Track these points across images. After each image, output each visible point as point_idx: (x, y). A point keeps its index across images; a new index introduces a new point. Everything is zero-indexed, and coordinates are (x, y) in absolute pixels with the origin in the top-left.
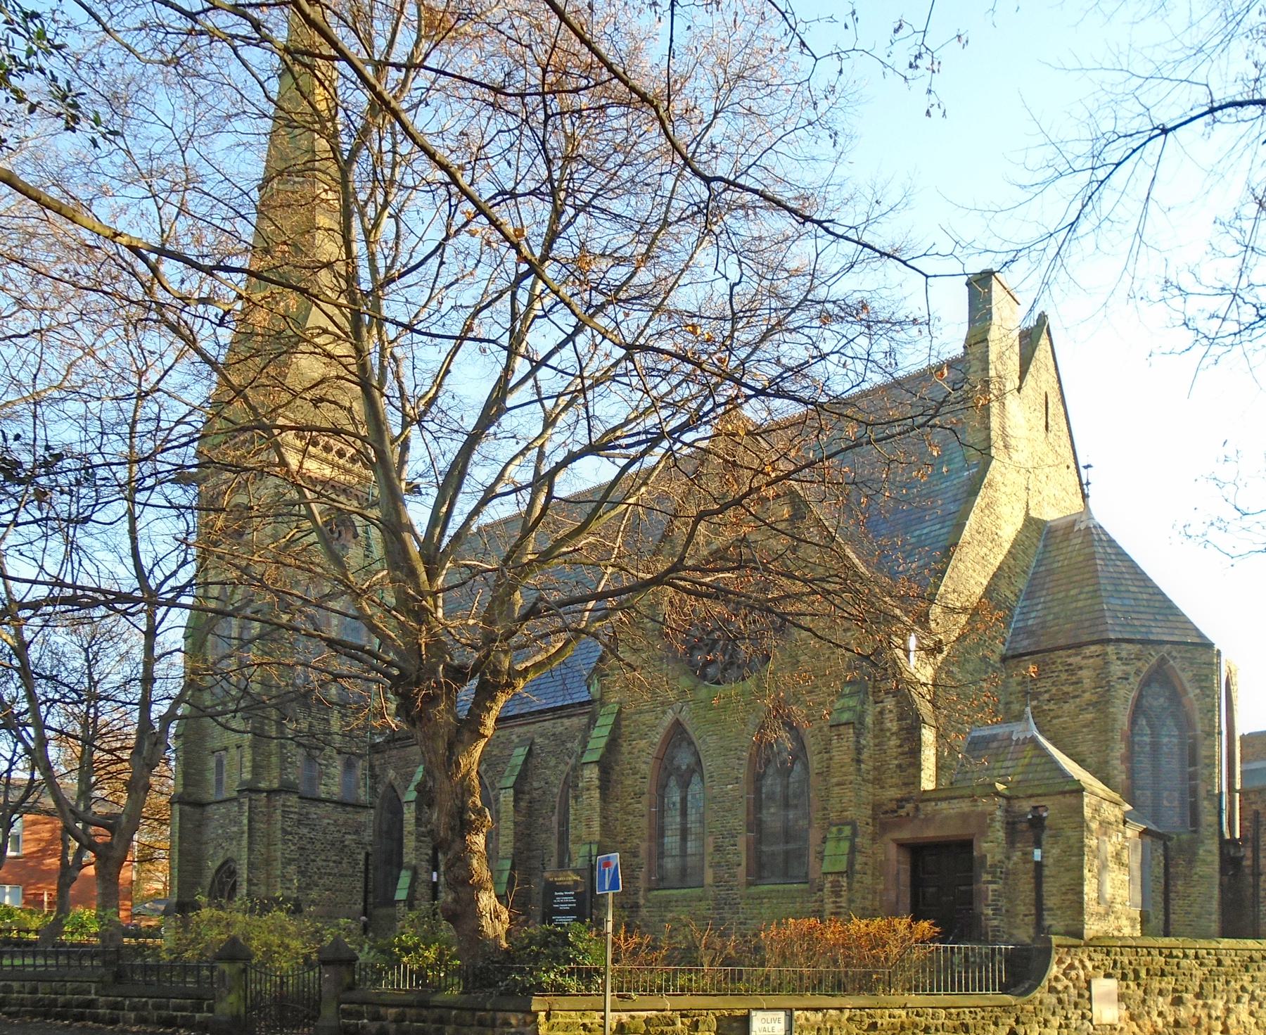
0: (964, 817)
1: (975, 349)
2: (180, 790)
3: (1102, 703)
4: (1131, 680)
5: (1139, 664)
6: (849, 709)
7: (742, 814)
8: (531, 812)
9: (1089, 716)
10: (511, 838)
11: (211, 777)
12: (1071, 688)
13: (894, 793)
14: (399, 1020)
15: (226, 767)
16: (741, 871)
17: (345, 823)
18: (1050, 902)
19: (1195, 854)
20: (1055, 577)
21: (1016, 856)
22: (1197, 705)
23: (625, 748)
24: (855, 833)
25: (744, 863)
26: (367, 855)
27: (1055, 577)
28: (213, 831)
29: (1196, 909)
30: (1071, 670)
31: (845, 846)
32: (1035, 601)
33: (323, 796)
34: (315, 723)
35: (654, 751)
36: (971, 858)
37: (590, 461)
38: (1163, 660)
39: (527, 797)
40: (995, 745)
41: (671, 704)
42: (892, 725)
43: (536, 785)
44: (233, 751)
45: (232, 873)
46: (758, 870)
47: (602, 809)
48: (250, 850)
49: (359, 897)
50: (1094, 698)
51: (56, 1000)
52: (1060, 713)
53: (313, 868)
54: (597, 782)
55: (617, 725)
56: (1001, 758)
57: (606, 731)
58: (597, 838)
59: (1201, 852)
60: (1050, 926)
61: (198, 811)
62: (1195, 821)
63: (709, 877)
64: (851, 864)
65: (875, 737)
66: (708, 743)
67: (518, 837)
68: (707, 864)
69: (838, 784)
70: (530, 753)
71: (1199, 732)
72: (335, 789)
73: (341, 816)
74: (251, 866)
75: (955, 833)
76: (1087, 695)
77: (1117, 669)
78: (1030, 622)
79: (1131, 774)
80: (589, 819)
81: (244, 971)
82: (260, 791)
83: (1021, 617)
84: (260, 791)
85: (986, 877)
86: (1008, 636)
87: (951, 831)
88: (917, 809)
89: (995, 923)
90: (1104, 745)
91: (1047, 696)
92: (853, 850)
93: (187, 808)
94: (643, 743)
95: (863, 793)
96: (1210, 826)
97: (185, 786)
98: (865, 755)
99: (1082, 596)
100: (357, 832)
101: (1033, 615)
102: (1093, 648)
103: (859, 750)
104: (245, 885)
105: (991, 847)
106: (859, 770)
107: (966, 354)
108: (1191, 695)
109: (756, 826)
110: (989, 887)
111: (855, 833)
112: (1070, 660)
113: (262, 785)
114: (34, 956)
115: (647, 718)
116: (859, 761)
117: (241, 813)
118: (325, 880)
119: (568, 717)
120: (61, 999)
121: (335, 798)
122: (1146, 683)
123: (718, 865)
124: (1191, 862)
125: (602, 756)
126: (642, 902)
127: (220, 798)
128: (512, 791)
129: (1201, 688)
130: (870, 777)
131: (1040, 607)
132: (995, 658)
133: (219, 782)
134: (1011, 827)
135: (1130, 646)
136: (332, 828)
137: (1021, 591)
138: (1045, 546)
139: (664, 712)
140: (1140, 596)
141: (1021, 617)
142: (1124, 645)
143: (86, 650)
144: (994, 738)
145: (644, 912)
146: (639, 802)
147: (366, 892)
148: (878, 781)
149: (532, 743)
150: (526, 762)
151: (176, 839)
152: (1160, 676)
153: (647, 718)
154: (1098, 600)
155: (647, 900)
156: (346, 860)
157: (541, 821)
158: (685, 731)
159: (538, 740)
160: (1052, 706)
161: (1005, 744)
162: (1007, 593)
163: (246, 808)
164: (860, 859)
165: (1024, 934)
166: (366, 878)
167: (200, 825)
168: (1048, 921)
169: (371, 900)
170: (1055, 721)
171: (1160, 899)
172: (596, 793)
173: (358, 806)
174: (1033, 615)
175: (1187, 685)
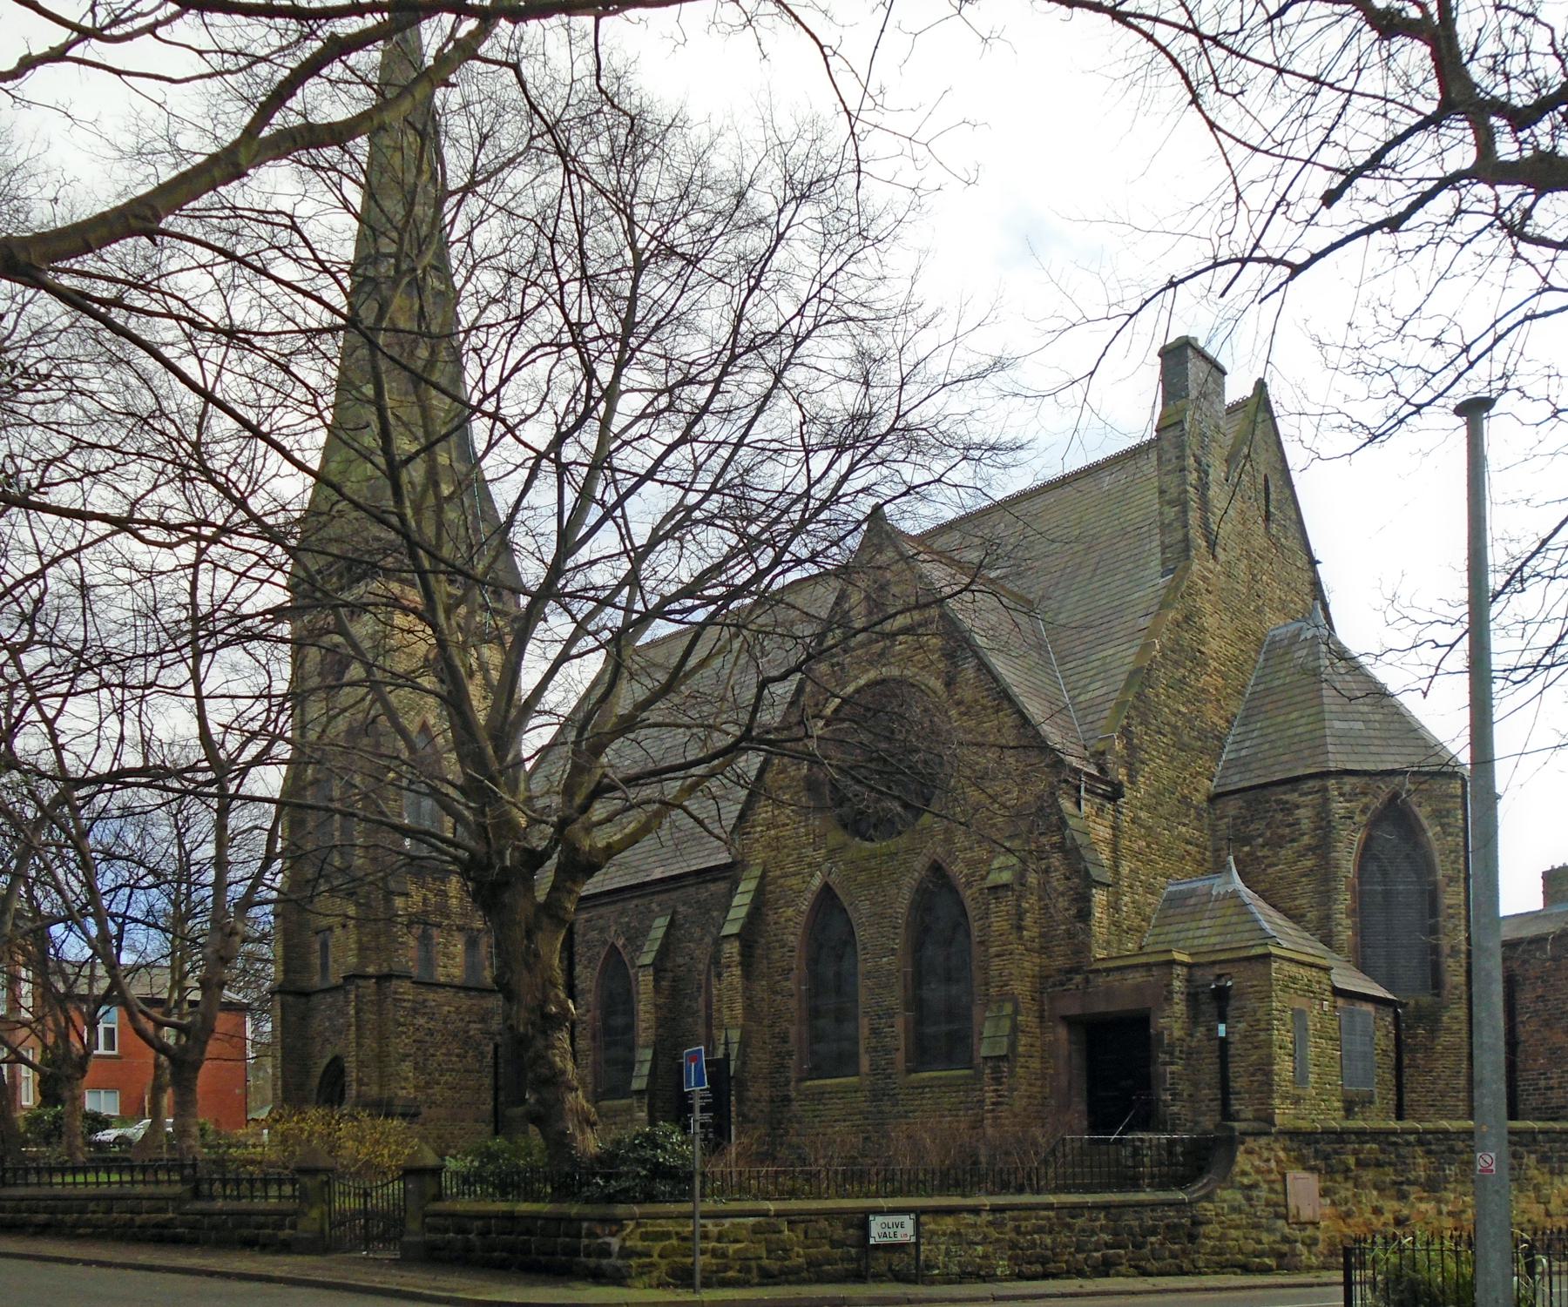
0: (1138, 989)
1: (1170, 434)
2: (281, 977)
3: (1323, 845)
4: (1357, 819)
5: (1365, 800)
6: (1007, 868)
7: (898, 991)
8: (675, 992)
9: (1309, 863)
10: (652, 1023)
11: (316, 960)
12: (1287, 830)
13: (1060, 962)
14: (484, 1233)
15: (332, 950)
16: (900, 1057)
17: (469, 1011)
18: (1238, 1084)
19: (1438, 1020)
20: (1275, 698)
21: (1201, 1032)
22: (1436, 845)
23: (772, 917)
24: (1016, 1012)
25: (902, 1046)
26: (496, 1047)
27: (1275, 698)
28: (319, 1023)
29: (1441, 1085)
30: (1288, 809)
31: (1006, 1025)
32: (1252, 727)
33: (442, 979)
34: (430, 896)
35: (802, 919)
36: (1148, 1037)
37: (570, 669)
38: (1395, 796)
39: (671, 974)
40: (1192, 901)
41: (818, 866)
42: (1057, 881)
43: (680, 960)
44: (338, 931)
45: (342, 1072)
46: (922, 1053)
47: (746, 989)
48: (359, 1045)
49: (488, 1096)
50: (1313, 842)
51: (132, 1220)
52: (1274, 860)
53: (432, 1065)
54: (737, 958)
55: (760, 892)
56: (1198, 916)
57: (747, 899)
58: (741, 1022)
59: (1445, 1019)
60: (1238, 1112)
61: (303, 1000)
62: (1436, 982)
63: (865, 1063)
64: (1013, 1045)
65: (1041, 899)
66: (860, 909)
67: (661, 1023)
68: (862, 1050)
69: (998, 956)
70: (672, 925)
71: (1440, 877)
72: (456, 972)
73: (464, 1001)
74: (361, 1064)
75: (1133, 1007)
76: (1306, 840)
77: (1339, 807)
78: (1243, 753)
79: (1361, 931)
80: (732, 1001)
81: (327, 1183)
82: (367, 977)
83: (1235, 747)
84: (367, 977)
85: (1163, 1057)
86: (1218, 770)
87: (1121, 1005)
88: (1087, 981)
89: (1175, 1109)
90: (1326, 897)
91: (1260, 840)
92: (1015, 1029)
93: (290, 999)
94: (790, 912)
95: (1026, 964)
96: (1456, 988)
97: (286, 972)
98: (1028, 920)
99: (1303, 721)
100: (483, 1020)
101: (1247, 744)
102: (1311, 783)
103: (1020, 915)
104: (354, 1086)
105: (1172, 1022)
106: (1021, 938)
107: (1159, 438)
108: (1430, 834)
109: (917, 1004)
110: (1170, 1070)
111: (1016, 1012)
112: (1284, 797)
113: (371, 970)
114: (120, 1171)
115: (793, 881)
116: (1020, 928)
117: (347, 1003)
118: (447, 1077)
119: (714, 880)
120: (138, 1219)
121: (457, 981)
122: (1373, 824)
123: (875, 1049)
124: (1433, 1032)
125: (743, 928)
126: (793, 1095)
127: (326, 986)
128: (651, 970)
129: (1442, 825)
130: (1036, 945)
131: (1255, 734)
132: (1199, 798)
133: (325, 966)
134: (1193, 998)
135: (1354, 780)
136: (453, 1016)
137: (1234, 716)
138: (1266, 660)
139: (812, 876)
140: (1372, 717)
141: (1235, 747)
142: (1347, 779)
143: (175, 816)
144: (1192, 893)
145: (795, 1106)
146: (787, 979)
147: (496, 1089)
148: (1044, 950)
149: (675, 913)
150: (667, 935)
151: (278, 1033)
152: (1396, 815)
153: (793, 881)
154: (1319, 725)
155: (798, 1091)
156: (471, 1053)
157: (687, 1002)
158: (835, 896)
159: (681, 909)
160: (1266, 852)
161: (1204, 899)
162: (1216, 719)
163: (352, 997)
164: (1023, 1040)
165: (1208, 1122)
166: (496, 1073)
167: (304, 1018)
168: (1236, 1106)
169: (502, 1099)
170: (1270, 871)
171: (1389, 1077)
172: (737, 971)
173: (483, 991)
174: (1247, 744)
175: (1425, 823)
